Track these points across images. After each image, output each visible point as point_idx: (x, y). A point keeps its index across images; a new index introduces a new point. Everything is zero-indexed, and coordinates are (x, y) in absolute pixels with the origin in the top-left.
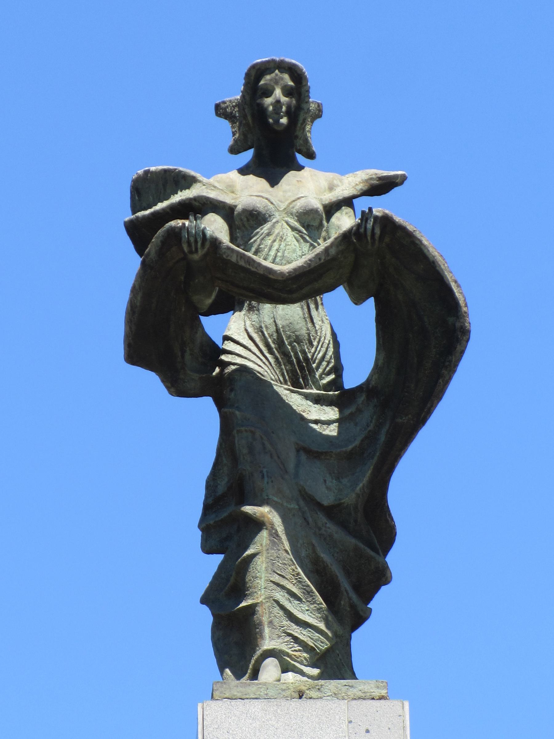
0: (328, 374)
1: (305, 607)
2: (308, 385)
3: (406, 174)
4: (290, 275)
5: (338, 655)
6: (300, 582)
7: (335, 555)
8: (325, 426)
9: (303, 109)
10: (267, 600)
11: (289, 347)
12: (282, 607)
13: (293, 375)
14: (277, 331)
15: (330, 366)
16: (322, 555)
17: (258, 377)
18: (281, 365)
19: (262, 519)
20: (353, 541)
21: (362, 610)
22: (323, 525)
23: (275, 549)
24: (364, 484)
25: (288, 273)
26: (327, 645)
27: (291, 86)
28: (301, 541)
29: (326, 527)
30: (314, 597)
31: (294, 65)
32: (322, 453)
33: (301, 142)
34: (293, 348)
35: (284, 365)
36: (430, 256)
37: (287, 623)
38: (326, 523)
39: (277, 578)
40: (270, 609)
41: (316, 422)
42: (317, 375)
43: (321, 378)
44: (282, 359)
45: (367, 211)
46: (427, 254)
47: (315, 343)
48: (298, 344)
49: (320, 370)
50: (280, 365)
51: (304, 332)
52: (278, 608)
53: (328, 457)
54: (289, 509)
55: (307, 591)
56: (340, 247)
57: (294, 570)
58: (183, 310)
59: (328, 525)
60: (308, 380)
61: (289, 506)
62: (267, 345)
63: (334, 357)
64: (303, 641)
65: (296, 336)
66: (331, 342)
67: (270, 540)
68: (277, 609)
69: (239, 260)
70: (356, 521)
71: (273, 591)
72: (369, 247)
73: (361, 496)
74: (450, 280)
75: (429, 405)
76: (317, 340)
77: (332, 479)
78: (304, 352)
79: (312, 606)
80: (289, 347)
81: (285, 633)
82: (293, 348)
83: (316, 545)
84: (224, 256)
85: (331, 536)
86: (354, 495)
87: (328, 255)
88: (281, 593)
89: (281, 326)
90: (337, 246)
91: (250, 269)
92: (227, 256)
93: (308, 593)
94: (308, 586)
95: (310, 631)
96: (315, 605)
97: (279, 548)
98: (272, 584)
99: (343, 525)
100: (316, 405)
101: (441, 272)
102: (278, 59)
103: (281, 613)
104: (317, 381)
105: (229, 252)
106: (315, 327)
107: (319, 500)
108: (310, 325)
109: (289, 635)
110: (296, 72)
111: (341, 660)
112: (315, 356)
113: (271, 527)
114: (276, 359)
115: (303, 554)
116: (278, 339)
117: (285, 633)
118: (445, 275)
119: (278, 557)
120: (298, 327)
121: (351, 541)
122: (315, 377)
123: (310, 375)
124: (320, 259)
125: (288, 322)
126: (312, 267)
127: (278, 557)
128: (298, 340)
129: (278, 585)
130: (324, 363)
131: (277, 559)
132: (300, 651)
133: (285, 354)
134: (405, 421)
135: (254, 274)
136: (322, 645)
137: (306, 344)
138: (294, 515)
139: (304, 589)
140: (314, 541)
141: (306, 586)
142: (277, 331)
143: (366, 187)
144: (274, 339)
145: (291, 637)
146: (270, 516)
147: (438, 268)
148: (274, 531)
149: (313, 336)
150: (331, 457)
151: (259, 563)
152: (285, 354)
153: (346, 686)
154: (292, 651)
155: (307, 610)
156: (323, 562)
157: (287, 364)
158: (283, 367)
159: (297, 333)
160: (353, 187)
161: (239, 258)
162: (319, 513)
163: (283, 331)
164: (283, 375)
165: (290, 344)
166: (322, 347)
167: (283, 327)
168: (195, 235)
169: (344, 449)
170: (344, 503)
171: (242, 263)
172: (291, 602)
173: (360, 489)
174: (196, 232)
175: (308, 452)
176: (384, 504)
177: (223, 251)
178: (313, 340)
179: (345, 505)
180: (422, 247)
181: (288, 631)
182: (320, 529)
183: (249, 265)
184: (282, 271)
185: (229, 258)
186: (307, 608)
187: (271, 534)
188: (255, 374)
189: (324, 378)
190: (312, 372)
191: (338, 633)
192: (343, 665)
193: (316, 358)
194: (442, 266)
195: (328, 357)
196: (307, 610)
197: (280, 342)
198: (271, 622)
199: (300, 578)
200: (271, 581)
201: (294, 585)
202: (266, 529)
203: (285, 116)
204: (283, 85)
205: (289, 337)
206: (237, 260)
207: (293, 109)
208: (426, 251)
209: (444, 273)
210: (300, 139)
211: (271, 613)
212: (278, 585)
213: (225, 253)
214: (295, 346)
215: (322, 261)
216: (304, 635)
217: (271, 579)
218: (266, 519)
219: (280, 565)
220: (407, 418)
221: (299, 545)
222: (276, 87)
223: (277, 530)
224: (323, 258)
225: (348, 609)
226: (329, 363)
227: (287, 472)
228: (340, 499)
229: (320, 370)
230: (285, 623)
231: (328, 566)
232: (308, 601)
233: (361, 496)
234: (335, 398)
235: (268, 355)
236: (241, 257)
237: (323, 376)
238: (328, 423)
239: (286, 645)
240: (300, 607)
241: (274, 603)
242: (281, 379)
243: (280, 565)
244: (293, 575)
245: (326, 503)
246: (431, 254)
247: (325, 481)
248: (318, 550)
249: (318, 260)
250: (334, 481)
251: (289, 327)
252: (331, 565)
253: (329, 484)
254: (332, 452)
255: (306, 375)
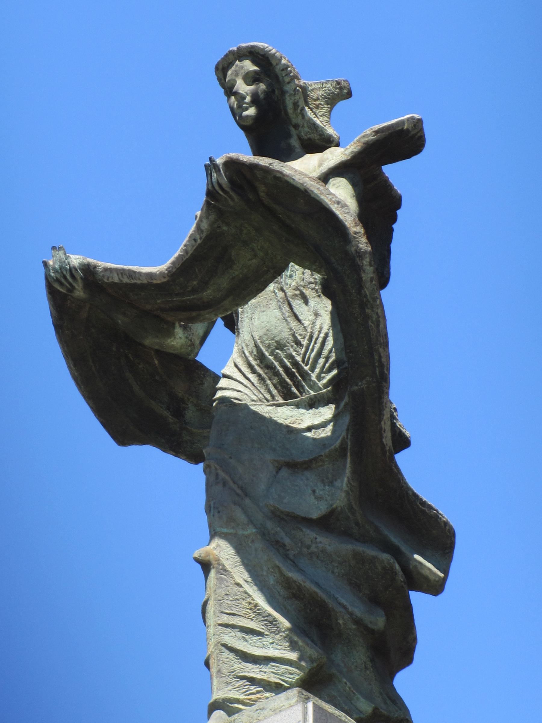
0: (329, 370)
1: (267, 640)
2: (304, 392)
3: (417, 116)
4: (169, 272)
5: (346, 684)
6: (259, 614)
7: (336, 570)
8: (320, 431)
9: (287, 92)
10: (216, 648)
11: (271, 358)
12: (232, 650)
13: (283, 387)
14: (256, 346)
15: (331, 361)
16: (290, 575)
17: (235, 404)
18: (265, 381)
19: (207, 558)
20: (350, 547)
21: (371, 622)
22: (312, 541)
23: (223, 586)
24: (348, 478)
25: (167, 270)
26: (298, 675)
27: (255, 72)
28: (265, 568)
29: (316, 543)
30: (278, 625)
31: (253, 47)
32: (311, 461)
33: (306, 129)
34: (277, 358)
35: (270, 379)
36: (299, 186)
37: (240, 666)
38: (316, 538)
39: (226, 619)
40: (218, 657)
41: (309, 429)
42: (314, 376)
43: (319, 378)
44: (266, 374)
45: (209, 163)
46: (295, 184)
47: (305, 342)
48: (282, 350)
49: (317, 370)
50: (265, 381)
51: (286, 334)
52: (227, 652)
53: (320, 464)
54: (246, 537)
55: (269, 622)
56: (210, 217)
57: (250, 603)
58: (156, 362)
59: (319, 539)
60: (303, 387)
61: (246, 533)
62: (250, 366)
63: (336, 350)
64: (262, 680)
65: (276, 342)
66: (331, 334)
67: (217, 579)
68: (227, 654)
69: (122, 279)
70: (357, 524)
71: (222, 635)
72: (232, 203)
73: (350, 493)
74: (329, 203)
75: (376, 357)
76: (307, 337)
77: (324, 486)
78: (290, 357)
79: (278, 637)
80: (271, 358)
81: (238, 677)
82: (277, 358)
83: (281, 565)
84: (106, 281)
85: (323, 551)
86: (343, 495)
87: (202, 231)
88: (233, 634)
89: (257, 338)
90: (208, 218)
91: (136, 283)
92: (108, 280)
93: (271, 622)
94: (270, 615)
95: (273, 666)
96: (281, 634)
97: (229, 584)
98: (220, 628)
99: (346, 534)
100: (310, 411)
101: (317, 198)
102: (235, 48)
103: (232, 656)
104: (314, 383)
105: (107, 274)
106: (303, 324)
107: (303, 515)
108: (293, 324)
109: (242, 678)
110: (258, 53)
111: (350, 688)
112: (307, 356)
113: (218, 564)
114: (259, 375)
115: (271, 581)
116: (258, 353)
117: (238, 677)
118: (322, 199)
119: (227, 595)
120: (275, 331)
121: (347, 548)
122: (310, 380)
123: (304, 380)
124: (195, 240)
125: (264, 330)
126: (190, 253)
127: (227, 595)
128: (280, 346)
129: (226, 626)
130: (321, 361)
131: (226, 597)
132: (258, 692)
133: (269, 367)
134: (364, 386)
135: (142, 287)
136: (291, 676)
137: (292, 346)
138: (253, 541)
139: (266, 620)
140: (277, 562)
141: (267, 616)
142: (256, 346)
143: (359, 148)
144: (255, 355)
145: (245, 680)
146: (215, 552)
147: (312, 195)
148: (220, 567)
149: (300, 335)
150: (323, 461)
151: (209, 609)
152: (269, 367)
153: (257, 710)
154: (246, 695)
155: (272, 643)
156: (295, 582)
157: (273, 377)
158: (268, 382)
159: (277, 339)
160: (342, 153)
161: (120, 275)
162: (304, 530)
163: (261, 342)
164: (269, 392)
165: (272, 354)
166: (315, 343)
167: (260, 338)
168: (60, 269)
169: (333, 447)
170: (337, 507)
171: (126, 280)
172: (246, 641)
173: (347, 485)
174: (70, 267)
175: (294, 466)
176: (407, 493)
177: (101, 274)
178: (302, 340)
179: (339, 509)
180: (286, 178)
181: (241, 674)
182: (309, 547)
183: (132, 279)
184: (161, 270)
185: (110, 280)
186: (271, 641)
187: (218, 572)
188: (232, 402)
189: (324, 378)
190: (305, 375)
191: (313, 657)
192: (354, 693)
193: (309, 358)
194: (316, 191)
195: (325, 352)
196: (272, 643)
197: (261, 357)
198: (219, 671)
199: (258, 610)
200: (220, 625)
201: (252, 620)
202: (213, 568)
203: (251, 107)
204: (244, 74)
205: (268, 347)
206: (119, 278)
207: (262, 96)
208: (292, 181)
209: (319, 197)
210: (303, 126)
211: (219, 660)
212: (226, 626)
213: (103, 276)
214: (278, 353)
215: (199, 241)
216: (265, 673)
217: (219, 622)
218: (211, 557)
219: (230, 602)
220: (364, 382)
221: (265, 573)
222: (237, 79)
223: (223, 565)
224: (198, 237)
225: (354, 627)
226: (327, 358)
227: (246, 495)
228: (331, 505)
229: (317, 370)
230: (236, 666)
231: (301, 585)
232: (272, 633)
233: (350, 493)
234: (330, 395)
235: (251, 376)
236: (122, 274)
237: (323, 375)
238: (323, 425)
239: (238, 691)
240: (261, 642)
241: (222, 648)
242: (268, 396)
243: (230, 602)
244: (251, 609)
245: (315, 515)
246: (298, 183)
247: (314, 491)
248: (284, 569)
249: (193, 242)
250: (327, 487)
251: (266, 334)
252: (304, 582)
253: (318, 492)
254: (322, 455)
255: (299, 382)
